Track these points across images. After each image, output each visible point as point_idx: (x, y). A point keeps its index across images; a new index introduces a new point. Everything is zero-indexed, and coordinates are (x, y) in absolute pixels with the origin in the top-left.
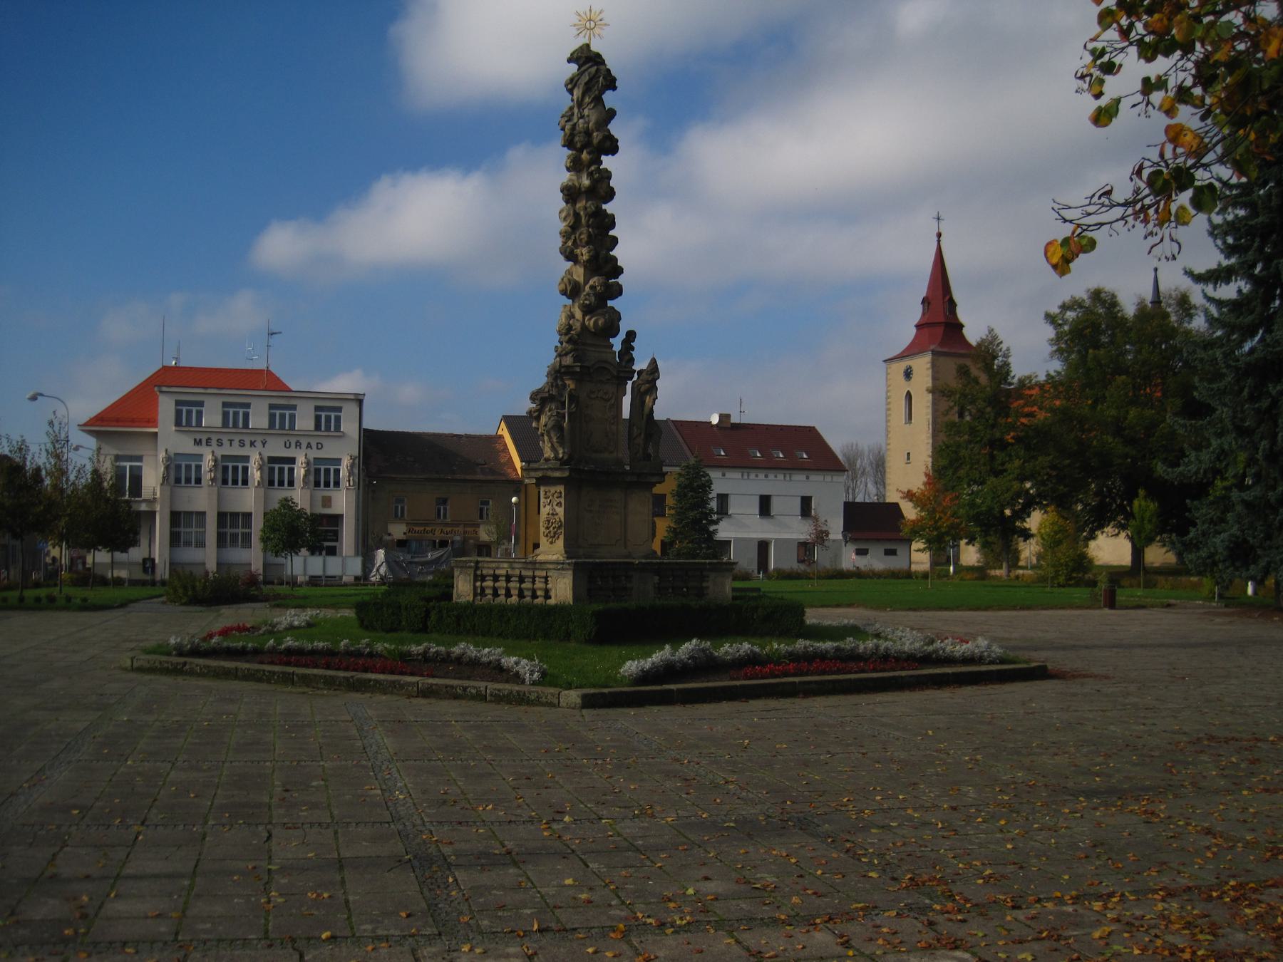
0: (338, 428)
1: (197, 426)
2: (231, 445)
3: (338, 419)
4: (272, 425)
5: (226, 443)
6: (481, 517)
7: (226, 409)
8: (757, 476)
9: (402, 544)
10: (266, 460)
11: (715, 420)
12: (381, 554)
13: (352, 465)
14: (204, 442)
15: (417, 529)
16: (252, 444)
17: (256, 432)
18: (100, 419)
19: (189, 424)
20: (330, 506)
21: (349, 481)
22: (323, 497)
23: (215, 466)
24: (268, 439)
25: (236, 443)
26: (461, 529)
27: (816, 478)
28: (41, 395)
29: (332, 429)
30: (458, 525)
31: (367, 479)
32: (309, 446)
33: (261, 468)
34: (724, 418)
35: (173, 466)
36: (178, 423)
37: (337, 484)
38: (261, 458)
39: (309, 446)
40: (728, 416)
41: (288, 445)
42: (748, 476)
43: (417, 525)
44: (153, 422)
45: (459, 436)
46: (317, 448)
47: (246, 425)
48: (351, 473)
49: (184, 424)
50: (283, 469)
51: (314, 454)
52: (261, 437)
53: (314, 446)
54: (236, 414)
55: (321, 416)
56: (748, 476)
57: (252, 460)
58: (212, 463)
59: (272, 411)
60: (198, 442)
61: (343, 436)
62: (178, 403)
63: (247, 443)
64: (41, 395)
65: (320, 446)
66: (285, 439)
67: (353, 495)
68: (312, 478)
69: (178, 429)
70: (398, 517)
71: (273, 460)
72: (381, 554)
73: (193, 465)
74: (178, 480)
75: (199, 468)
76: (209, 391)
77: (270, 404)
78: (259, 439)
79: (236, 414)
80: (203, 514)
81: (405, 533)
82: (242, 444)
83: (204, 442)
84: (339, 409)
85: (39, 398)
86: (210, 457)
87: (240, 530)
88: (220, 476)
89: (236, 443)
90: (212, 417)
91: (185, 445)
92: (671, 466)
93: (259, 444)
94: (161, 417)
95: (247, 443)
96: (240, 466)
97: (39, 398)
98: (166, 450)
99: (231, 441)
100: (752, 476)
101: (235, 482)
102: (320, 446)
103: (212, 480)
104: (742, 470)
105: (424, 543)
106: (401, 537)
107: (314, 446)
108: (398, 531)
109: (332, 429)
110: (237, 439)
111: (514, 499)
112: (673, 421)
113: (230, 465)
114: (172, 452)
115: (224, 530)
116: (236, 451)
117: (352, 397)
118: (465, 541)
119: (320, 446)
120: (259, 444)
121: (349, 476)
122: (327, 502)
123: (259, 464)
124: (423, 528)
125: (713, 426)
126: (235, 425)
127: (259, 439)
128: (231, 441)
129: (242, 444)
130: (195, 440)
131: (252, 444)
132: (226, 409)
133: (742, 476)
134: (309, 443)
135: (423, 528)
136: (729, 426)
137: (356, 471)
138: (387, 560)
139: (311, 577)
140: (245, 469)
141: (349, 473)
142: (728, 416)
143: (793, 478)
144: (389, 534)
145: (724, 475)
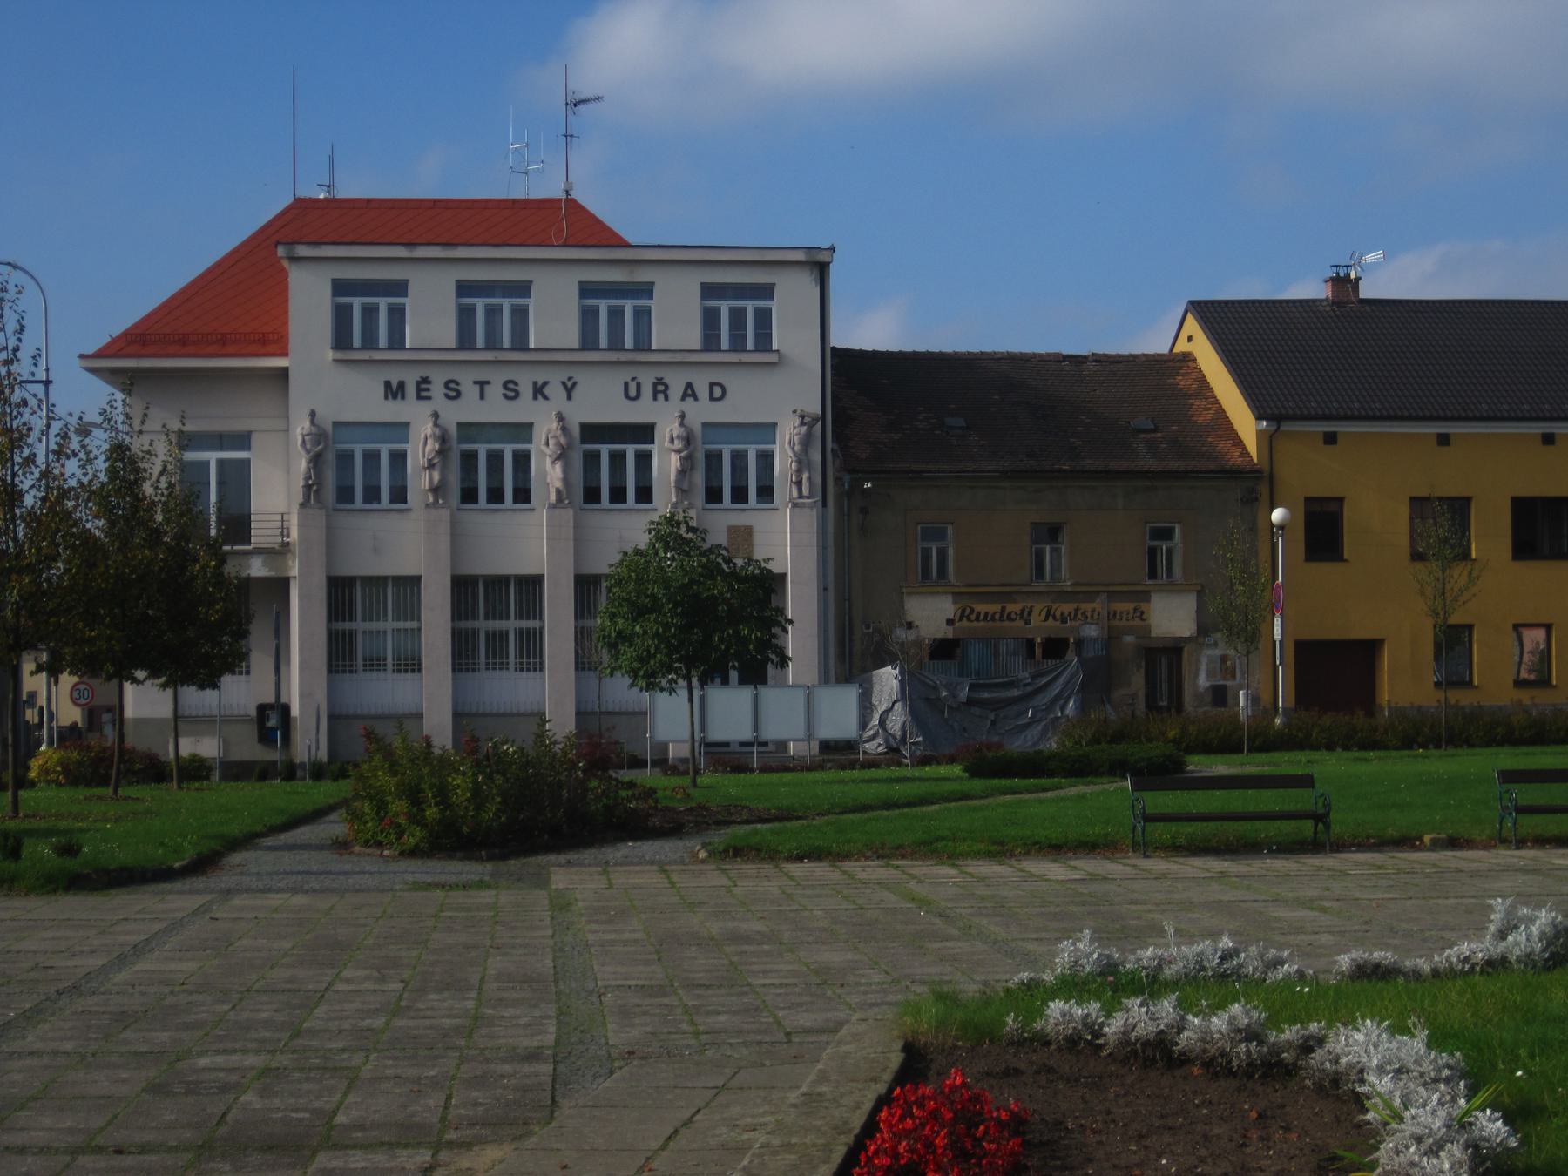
2: (482, 397)
3: (764, 318)
5: (469, 390)
6: (1153, 574)
9: (944, 649)
10: (576, 432)
14: (411, 390)
15: (981, 608)
16: (539, 391)
17: (549, 359)
19: (370, 342)
21: (799, 483)
24: (580, 376)
25: (495, 391)
29: (750, 344)
30: (1090, 596)
31: (847, 478)
32: (689, 392)
33: (563, 455)
35: (331, 457)
36: (341, 340)
37: (766, 492)
38: (564, 429)
39: (689, 392)
41: (633, 393)
44: (276, 342)
46: (712, 398)
51: (703, 412)
53: (702, 390)
57: (540, 435)
58: (433, 446)
60: (394, 391)
61: (778, 363)
62: (340, 287)
63: (526, 390)
65: (718, 392)
66: (625, 375)
67: (810, 518)
68: (699, 479)
69: (340, 355)
70: (931, 578)
71: (593, 432)
73: (508, 450)
75: (399, 459)
78: (555, 379)
80: (532, 584)
81: (950, 622)
83: (411, 390)
84: (766, 291)
86: (429, 428)
87: (512, 625)
89: (495, 391)
93: (556, 391)
95: (526, 390)
98: (313, 414)
99: (482, 384)
101: (496, 495)
102: (718, 393)
105: (1003, 648)
107: (702, 390)
109: (750, 344)
110: (497, 378)
116: (497, 410)
117: (800, 256)
118: (1111, 638)
119: (718, 392)
120: (556, 391)
123: (558, 444)
126: (493, 344)
128: (482, 384)
130: (388, 384)
131: (539, 391)
134: (689, 386)
137: (816, 456)
141: (799, 462)
144: (910, 625)
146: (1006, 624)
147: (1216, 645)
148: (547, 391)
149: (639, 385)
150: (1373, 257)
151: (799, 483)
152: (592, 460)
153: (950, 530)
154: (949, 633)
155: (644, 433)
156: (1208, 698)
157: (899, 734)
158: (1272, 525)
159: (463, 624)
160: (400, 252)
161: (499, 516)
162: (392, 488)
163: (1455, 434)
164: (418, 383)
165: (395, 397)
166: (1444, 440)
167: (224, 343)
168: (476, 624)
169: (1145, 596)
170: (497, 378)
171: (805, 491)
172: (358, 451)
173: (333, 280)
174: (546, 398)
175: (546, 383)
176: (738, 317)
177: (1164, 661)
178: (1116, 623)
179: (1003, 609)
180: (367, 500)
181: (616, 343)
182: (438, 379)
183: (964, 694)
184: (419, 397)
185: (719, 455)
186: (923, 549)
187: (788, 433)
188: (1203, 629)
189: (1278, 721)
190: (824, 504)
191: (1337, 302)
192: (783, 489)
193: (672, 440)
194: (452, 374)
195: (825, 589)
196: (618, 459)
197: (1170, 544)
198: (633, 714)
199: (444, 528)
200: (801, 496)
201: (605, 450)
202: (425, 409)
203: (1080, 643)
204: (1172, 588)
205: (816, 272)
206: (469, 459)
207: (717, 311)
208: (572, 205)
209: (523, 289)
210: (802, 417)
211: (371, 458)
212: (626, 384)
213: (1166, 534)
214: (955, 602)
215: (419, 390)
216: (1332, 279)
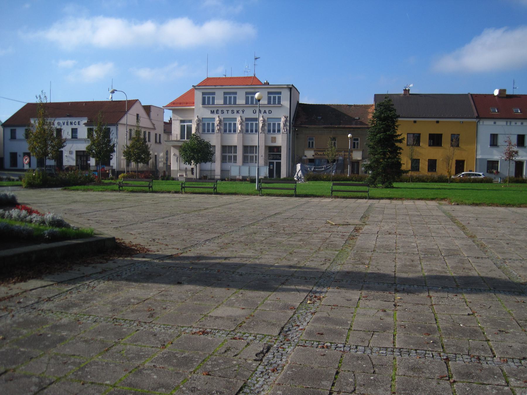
0: (279, 102)
1: (278, 104)
2: (228, 113)
3: (279, 98)
4: (247, 103)
5: (225, 112)
6: (354, 147)
7: (204, 96)
8: (516, 123)
9: (311, 161)
10: (244, 119)
11: (496, 93)
12: (299, 166)
13: (286, 121)
14: (215, 112)
15: (319, 153)
16: (238, 112)
17: (240, 106)
18: (173, 103)
19: (209, 104)
20: (275, 142)
21: (284, 129)
22: (272, 138)
23: (219, 123)
24: (245, 109)
25: (230, 112)
26: (343, 153)
27: (501, 123)
28: (116, 91)
29: (277, 103)
30: (341, 151)
31: (293, 128)
32: (265, 112)
33: (241, 124)
34: (502, 92)
35: (201, 124)
36: (204, 103)
37: (279, 131)
38: (241, 119)
39: (265, 112)
40: (505, 90)
41: (255, 112)
42: (510, 123)
43: (320, 151)
44: (193, 104)
45: (350, 106)
46: (269, 113)
47: (235, 103)
48: (285, 125)
49: (206, 103)
50: (253, 124)
51: (267, 116)
52: (241, 109)
53: (267, 112)
54: (230, 98)
55: (271, 97)
56: (510, 123)
57: (238, 120)
58: (218, 122)
59: (247, 95)
60: (212, 112)
61: (282, 106)
62: (203, 94)
63: (235, 112)
64: (116, 91)
65: (270, 112)
66: (253, 109)
67: (285, 136)
68: (266, 128)
69: (203, 106)
70: (310, 146)
71: (247, 119)
72: (299, 166)
73: (232, 123)
74: (225, 131)
75: (213, 124)
76: (217, 87)
77: (268, 92)
78: (241, 110)
79: (230, 98)
80: (235, 147)
81: (313, 156)
82: (233, 112)
83: (215, 112)
84: (280, 93)
85: (115, 92)
86: (240, 118)
87: (233, 154)
88: (222, 128)
89: (230, 112)
90: (219, 101)
91: (206, 113)
92: (462, 118)
93: (241, 112)
94: (196, 101)
95: (235, 112)
96: (232, 123)
97: (115, 92)
98: (198, 116)
99: (228, 111)
100: (513, 123)
101: (230, 131)
102: (270, 112)
103: (218, 130)
104: (507, 120)
105: (323, 161)
106: (312, 157)
107: (267, 112)
108: (310, 154)
109: (277, 103)
110: (230, 109)
111: (349, 135)
112: (471, 95)
113: (228, 123)
114: (200, 118)
115: (247, 154)
116: (230, 115)
117: (286, 86)
118: (344, 159)
119: (270, 112)
120: (241, 112)
121: (284, 127)
122: (274, 140)
123: (240, 121)
124: (322, 153)
125: (495, 96)
126: (230, 104)
127: (241, 110)
128: (228, 111)
129: (233, 112)
130: (211, 111)
131: (238, 112)
132: (204, 96)
133: (507, 123)
134: (265, 111)
135: (322, 153)
136: (505, 96)
137: (288, 124)
138: (301, 169)
139: (243, 177)
140: (235, 124)
141: (284, 125)
142: (505, 90)
143: (484, 124)
144: (306, 156)
145: (495, 123)
146: (324, 156)
147: (366, 161)
148: (239, 112)
149: (256, 111)
150: (411, 85)
151: (284, 129)
152: (247, 124)
153: (314, 138)
154: (313, 158)
155: (256, 119)
156: (364, 172)
157: (300, 176)
158: (349, 138)
159: (224, 154)
160: (214, 87)
161: (230, 135)
162: (212, 130)
163: (441, 121)
164: (216, 111)
165: (212, 113)
166: (438, 122)
167: (187, 104)
168: (226, 154)
169: (352, 152)
170: (230, 109)
171: (285, 131)
172: (228, 123)
173: (202, 92)
174: (239, 113)
175: (239, 111)
176: (274, 98)
177: (356, 164)
178: (346, 157)
179: (324, 153)
180: (208, 132)
181: (230, 104)
182: (220, 110)
183: (312, 169)
184: (217, 113)
185: (270, 124)
186: (309, 142)
187: (283, 119)
188: (363, 158)
189: (348, 175)
190: (290, 133)
191: (404, 94)
192: (282, 130)
193: (261, 121)
194: (232, 109)
195: (289, 149)
196: (252, 124)
197: (357, 142)
198: (227, 171)
199: (219, 138)
200: (284, 131)
201: (250, 123)
202: (217, 115)
203: (338, 160)
204: (357, 150)
205: (289, 90)
206: (225, 124)
207: (271, 97)
208: (255, 77)
209: (236, 93)
210: (285, 117)
211: (208, 124)
212: (253, 111)
213: (357, 140)
214: (314, 152)
215: (217, 112)
216: (404, 90)
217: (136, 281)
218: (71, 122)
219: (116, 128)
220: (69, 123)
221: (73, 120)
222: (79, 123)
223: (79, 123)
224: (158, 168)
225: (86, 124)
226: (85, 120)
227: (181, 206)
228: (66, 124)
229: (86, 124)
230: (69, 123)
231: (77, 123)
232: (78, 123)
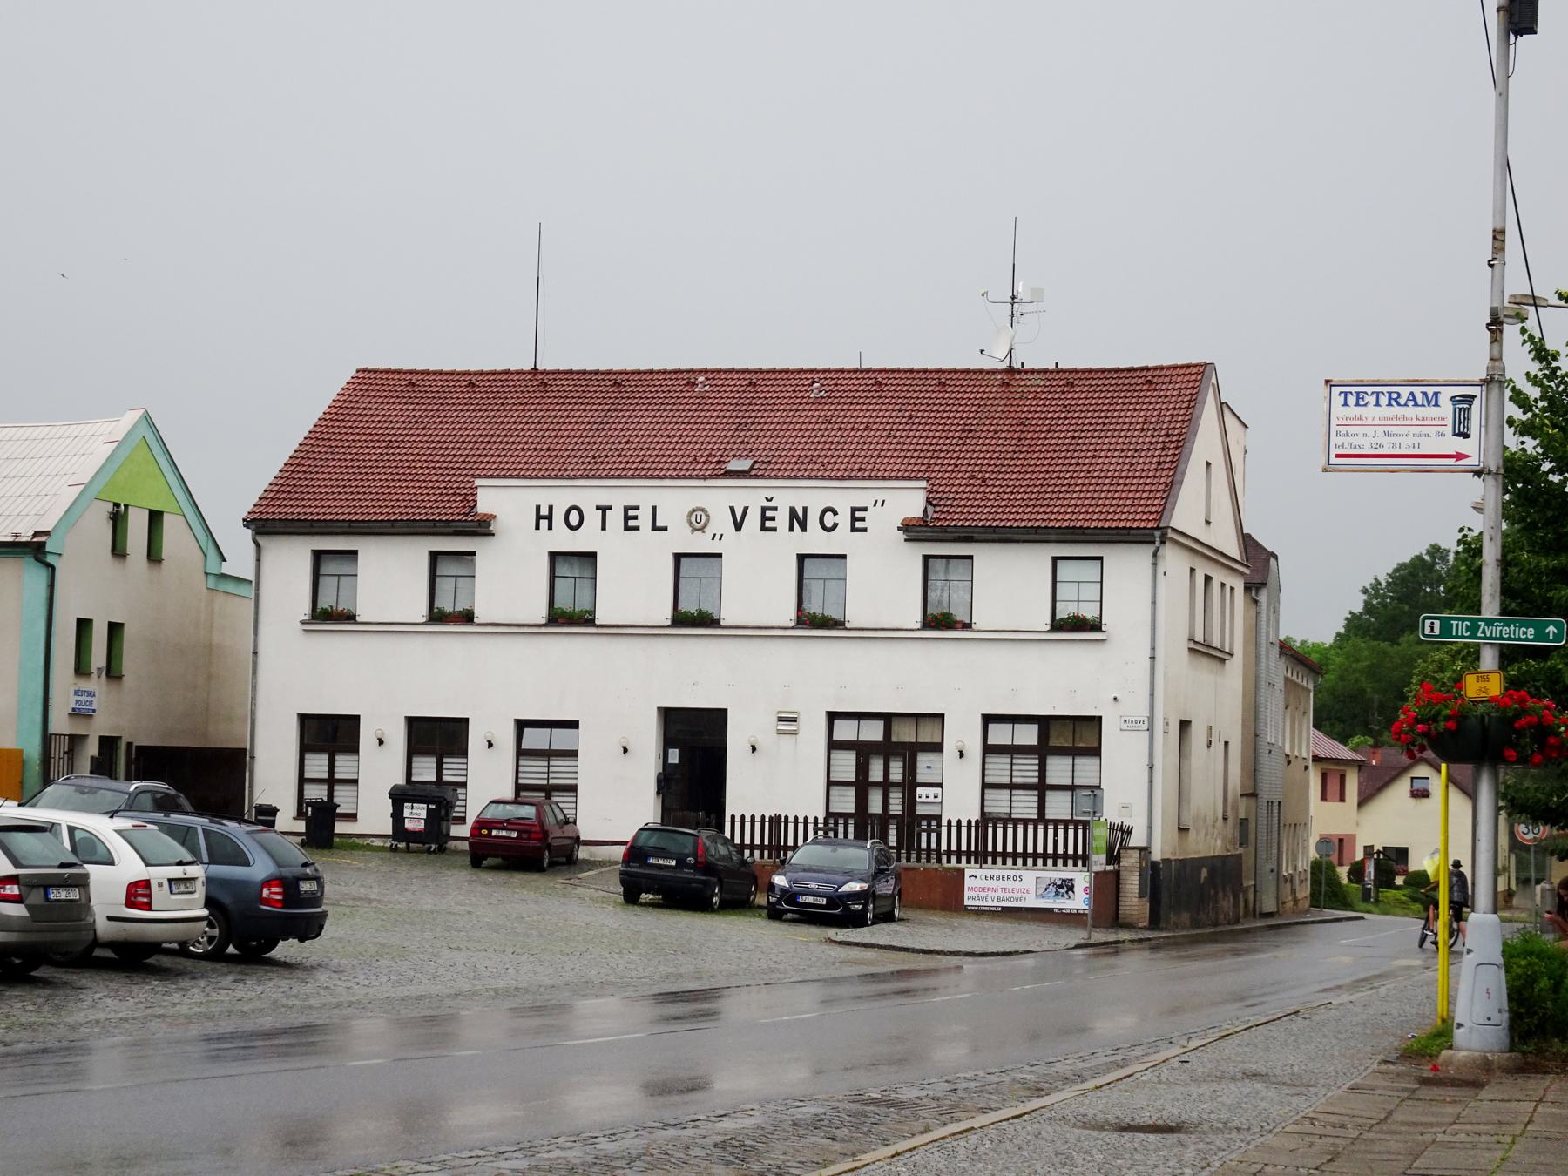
99: (604, 509)
128: (604, 509)
217: (1502, 578)
218: (793, 513)
219: (1150, 560)
220: (782, 519)
221: (812, 496)
222: (856, 516)
223: (856, 516)
224: (546, 828)
225: (914, 531)
226: (909, 501)
227: (11, 1058)
228: (753, 519)
229: (914, 531)
230: (782, 519)
231: (844, 519)
232: (854, 519)
